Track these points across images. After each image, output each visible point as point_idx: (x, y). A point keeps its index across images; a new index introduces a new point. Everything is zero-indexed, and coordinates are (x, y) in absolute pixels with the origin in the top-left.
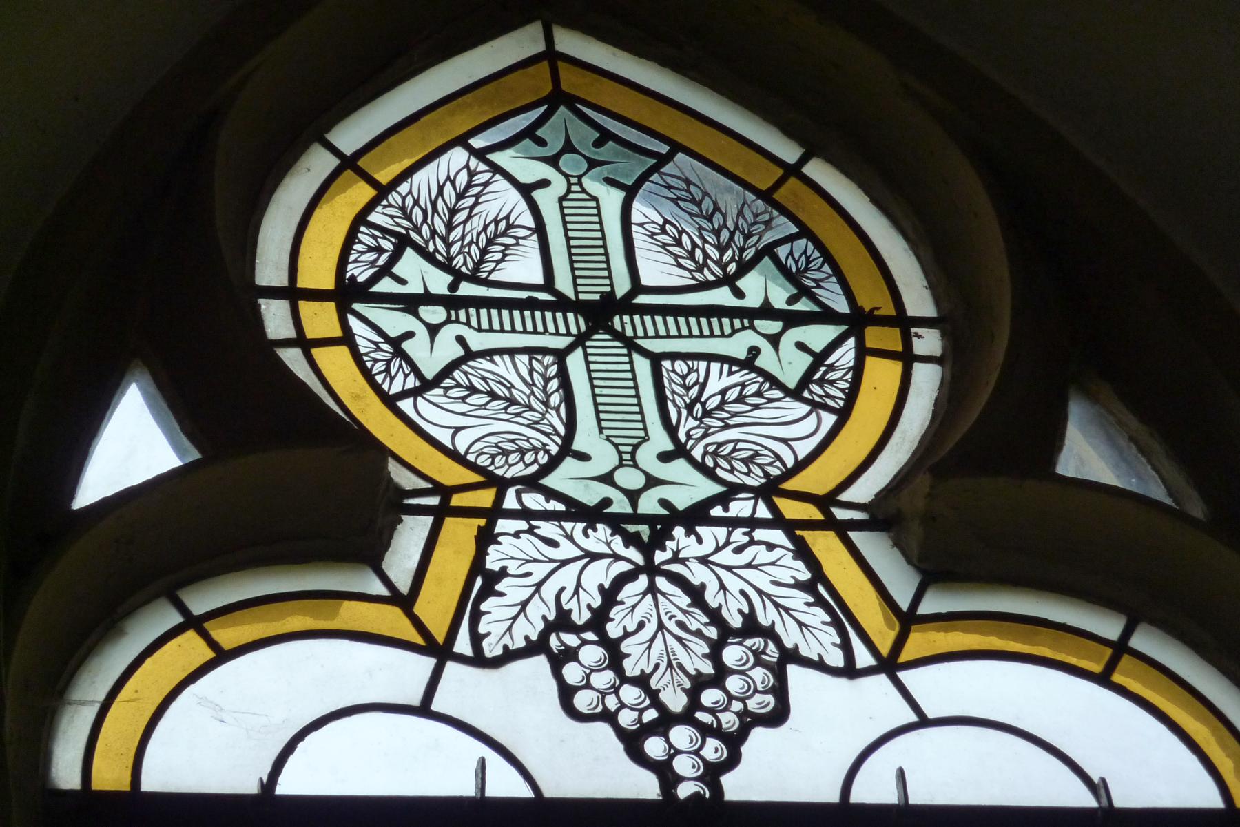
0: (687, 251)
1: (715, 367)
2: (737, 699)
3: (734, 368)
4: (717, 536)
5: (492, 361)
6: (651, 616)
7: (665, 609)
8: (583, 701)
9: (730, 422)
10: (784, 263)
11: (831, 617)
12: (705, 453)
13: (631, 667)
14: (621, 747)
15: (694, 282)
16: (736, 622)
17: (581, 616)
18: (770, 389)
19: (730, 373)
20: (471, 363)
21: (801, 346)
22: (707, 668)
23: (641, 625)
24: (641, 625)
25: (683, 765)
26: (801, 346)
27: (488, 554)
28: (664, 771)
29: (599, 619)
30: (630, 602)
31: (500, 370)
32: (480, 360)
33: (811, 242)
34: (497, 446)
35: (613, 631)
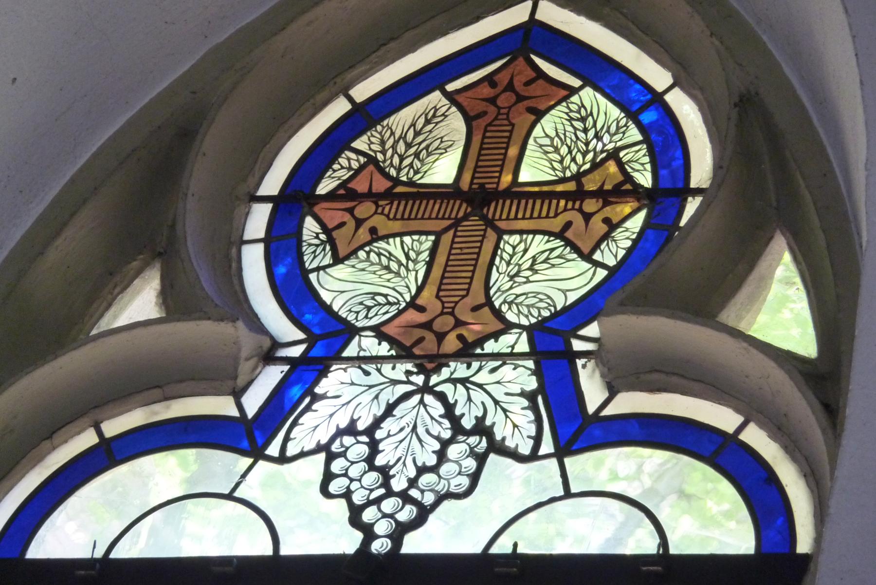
0: (587, 139)
1: (539, 237)
2: (445, 479)
3: (552, 238)
4: (511, 437)
5: (388, 243)
6: (411, 423)
7: (422, 419)
8: (335, 486)
9: (531, 279)
10: (94, 332)
11: (492, 339)
12: (505, 302)
13: (380, 461)
14: (348, 514)
15: (556, 178)
16: (468, 423)
17: (361, 426)
18: (570, 253)
19: (548, 241)
20: (375, 244)
21: (342, 225)
22: (432, 461)
23: (402, 430)
24: (402, 430)
25: (382, 528)
26: (342, 225)
27: (327, 377)
28: (369, 534)
29: (370, 431)
30: (398, 416)
31: (391, 248)
32: (380, 242)
33: (591, 165)
34: (361, 303)
35: (379, 434)
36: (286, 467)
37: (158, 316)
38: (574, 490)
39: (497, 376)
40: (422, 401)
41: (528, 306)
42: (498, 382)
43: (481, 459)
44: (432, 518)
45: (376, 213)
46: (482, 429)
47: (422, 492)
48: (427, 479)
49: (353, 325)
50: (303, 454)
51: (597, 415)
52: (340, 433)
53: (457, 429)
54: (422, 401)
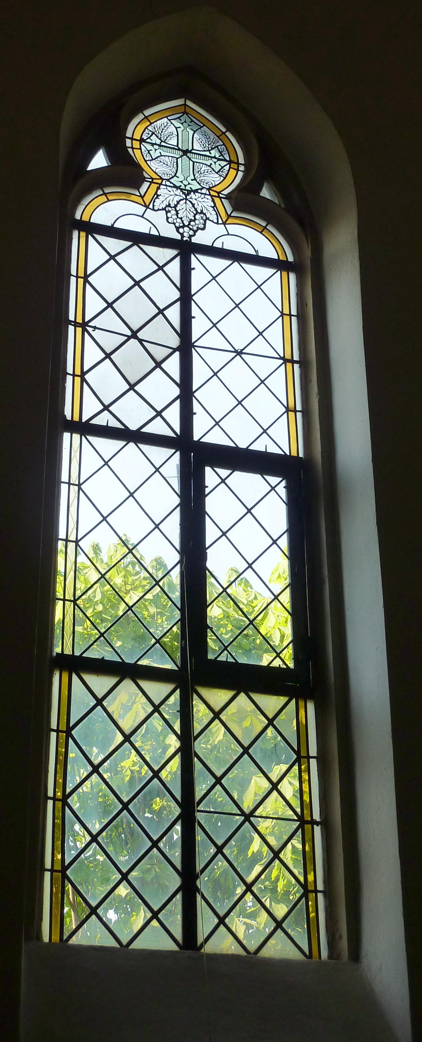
16: (199, 211)
22: (193, 218)
23: (183, 209)
24: (183, 209)
28: (182, 235)
29: (175, 206)
30: (181, 204)
31: (166, 159)
36: (145, 127)
37: (106, 165)
38: (231, 169)
39: (203, 200)
40: (186, 203)
41: (206, 136)
42: (203, 202)
43: (205, 221)
44: (197, 233)
45: (159, 149)
46: (202, 212)
47: (192, 226)
48: (192, 223)
49: (207, 638)
50: (159, 210)
51: (181, 946)
52: (167, 206)
53: (197, 212)
54: (186, 203)
